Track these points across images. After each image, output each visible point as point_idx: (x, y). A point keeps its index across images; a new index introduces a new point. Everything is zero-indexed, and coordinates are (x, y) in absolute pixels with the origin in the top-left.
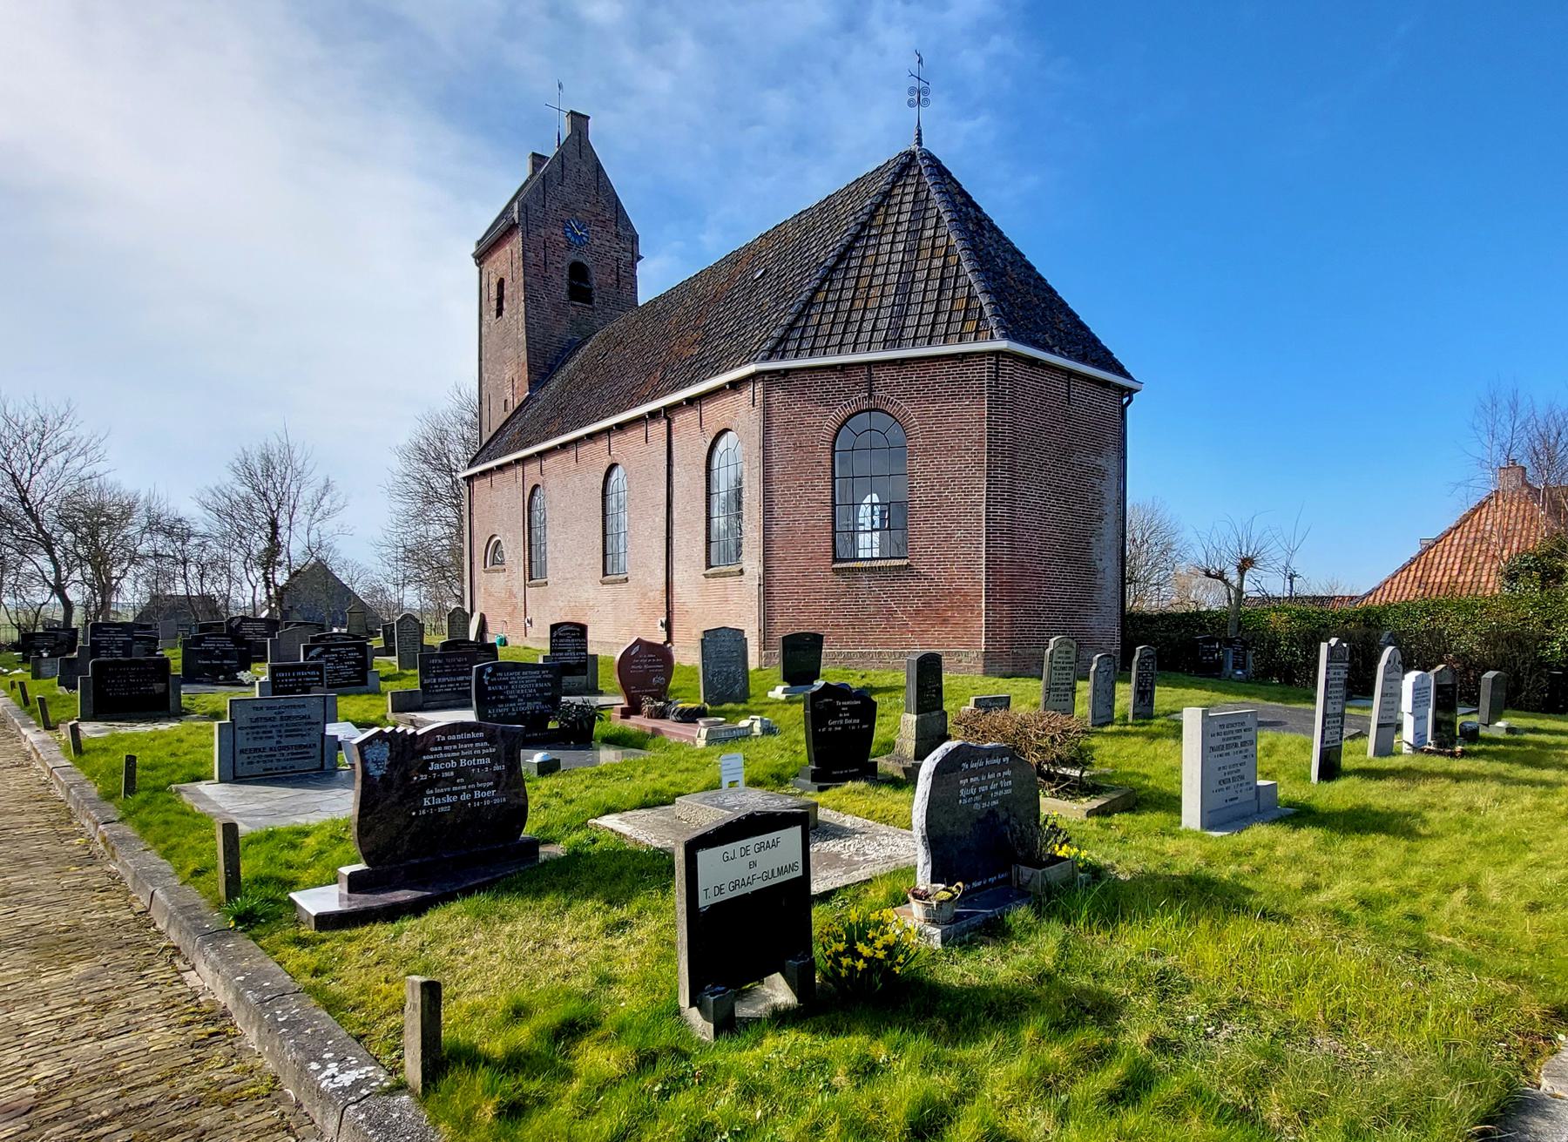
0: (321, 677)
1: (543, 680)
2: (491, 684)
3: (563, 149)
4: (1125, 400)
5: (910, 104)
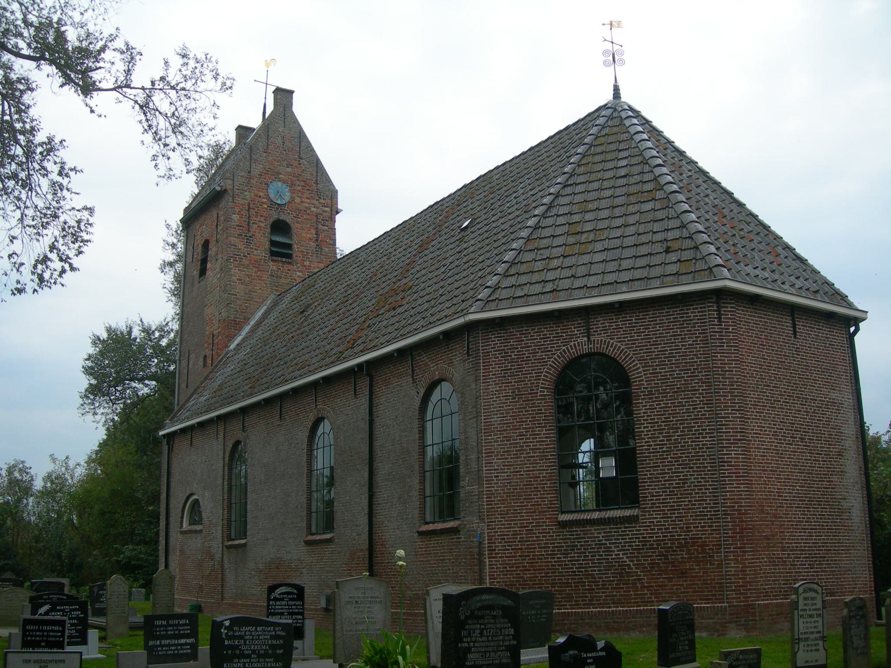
0: (63, 632)
1: (276, 637)
2: (229, 638)
3: (268, 122)
4: (852, 329)
5: (605, 63)
